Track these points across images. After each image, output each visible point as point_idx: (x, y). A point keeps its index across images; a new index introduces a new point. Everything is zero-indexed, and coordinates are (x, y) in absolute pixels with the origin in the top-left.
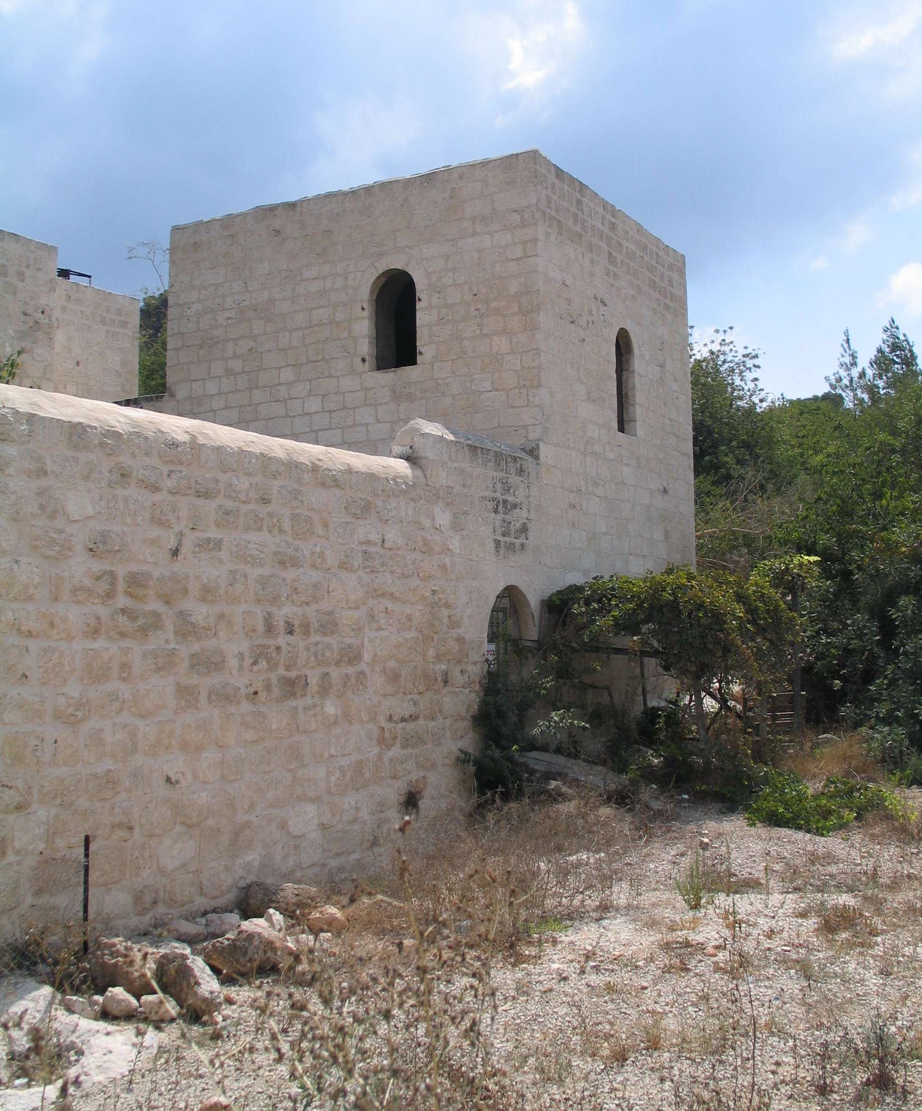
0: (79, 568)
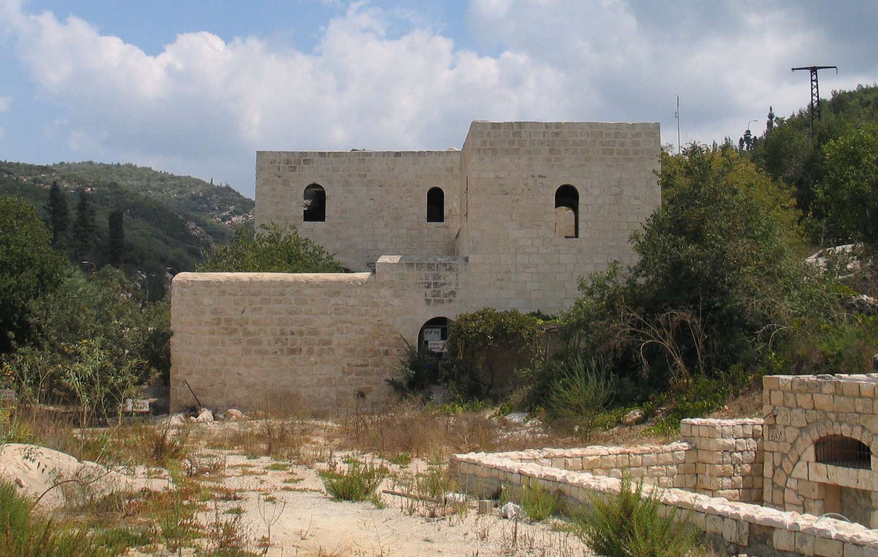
0: (208, 317)
